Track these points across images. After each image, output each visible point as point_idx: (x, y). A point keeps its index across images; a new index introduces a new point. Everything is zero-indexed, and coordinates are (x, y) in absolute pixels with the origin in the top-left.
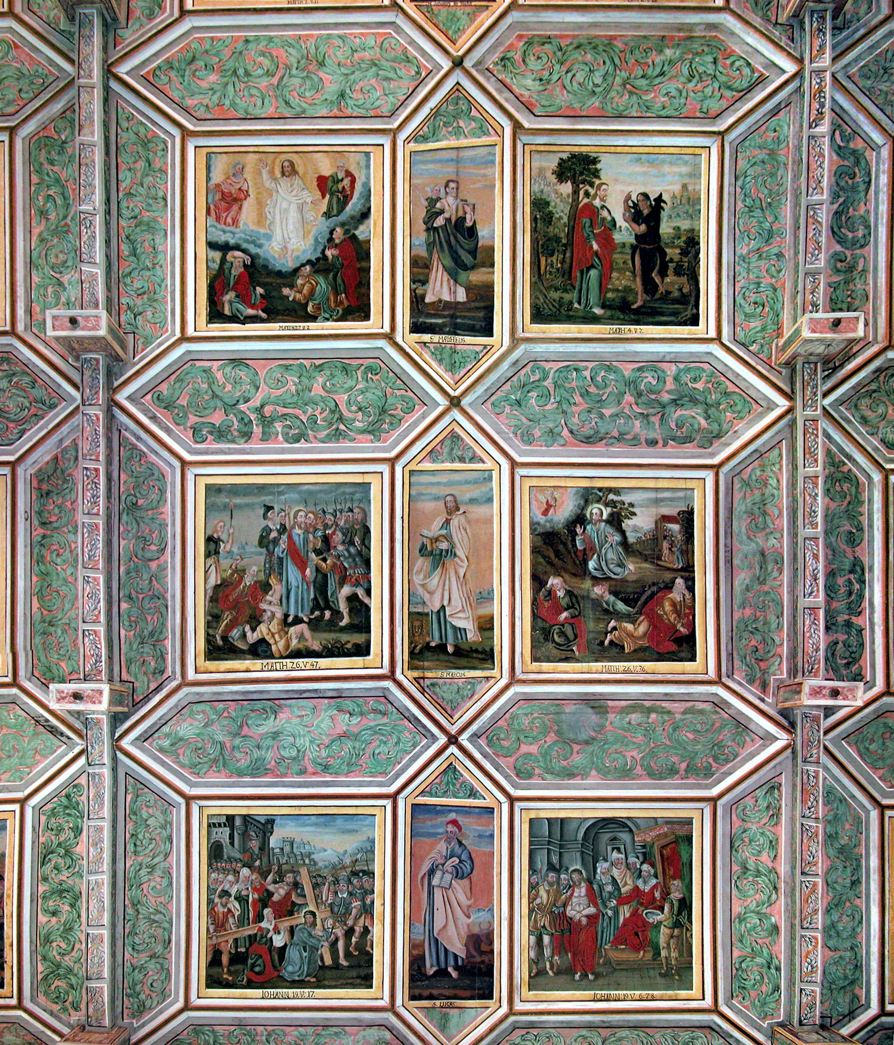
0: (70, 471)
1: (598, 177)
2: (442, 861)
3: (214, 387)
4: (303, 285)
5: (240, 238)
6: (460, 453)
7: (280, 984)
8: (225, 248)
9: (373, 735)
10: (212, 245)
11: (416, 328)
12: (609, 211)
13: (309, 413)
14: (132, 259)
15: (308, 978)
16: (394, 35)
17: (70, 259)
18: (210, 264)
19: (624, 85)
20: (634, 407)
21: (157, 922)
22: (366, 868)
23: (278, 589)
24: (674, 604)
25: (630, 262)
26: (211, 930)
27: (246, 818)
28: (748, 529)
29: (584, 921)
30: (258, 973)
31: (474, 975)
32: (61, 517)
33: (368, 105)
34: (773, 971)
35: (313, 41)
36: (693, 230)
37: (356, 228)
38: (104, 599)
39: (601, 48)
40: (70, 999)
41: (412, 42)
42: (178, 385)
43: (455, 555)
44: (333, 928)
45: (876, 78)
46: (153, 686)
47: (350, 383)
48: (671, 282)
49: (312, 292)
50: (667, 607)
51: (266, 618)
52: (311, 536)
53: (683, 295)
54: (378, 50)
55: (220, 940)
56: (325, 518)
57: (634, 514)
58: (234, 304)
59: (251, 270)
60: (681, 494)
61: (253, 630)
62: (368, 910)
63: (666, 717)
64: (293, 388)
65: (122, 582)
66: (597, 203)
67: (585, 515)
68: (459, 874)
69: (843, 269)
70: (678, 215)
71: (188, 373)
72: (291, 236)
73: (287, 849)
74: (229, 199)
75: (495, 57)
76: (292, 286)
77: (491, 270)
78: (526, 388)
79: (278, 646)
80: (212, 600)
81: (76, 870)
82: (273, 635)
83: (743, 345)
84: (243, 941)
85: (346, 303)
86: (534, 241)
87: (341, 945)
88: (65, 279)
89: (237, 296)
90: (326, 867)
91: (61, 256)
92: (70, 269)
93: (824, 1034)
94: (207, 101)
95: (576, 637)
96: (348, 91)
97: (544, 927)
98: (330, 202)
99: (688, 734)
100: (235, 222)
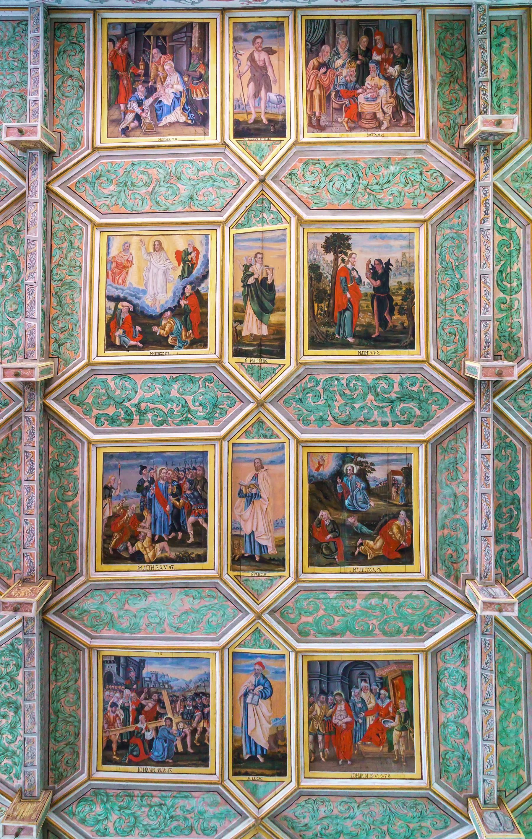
1: (350, 249)
2: (253, 688)
3: (108, 392)
4: (166, 325)
5: (127, 293)
6: (263, 432)
7: (149, 763)
8: (116, 300)
9: (207, 610)
10: (109, 298)
11: (237, 353)
12: (357, 272)
16: (224, 160)
17: (20, 308)
18: (107, 311)
19: (365, 188)
20: (374, 402)
21: (69, 722)
22: (204, 691)
24: (399, 528)
25: (370, 306)
26: (106, 727)
27: (127, 658)
28: (446, 479)
29: (344, 726)
30: (136, 756)
32: (10, 475)
33: (207, 204)
34: (466, 761)
35: (174, 164)
36: (409, 283)
37: (199, 286)
39: (350, 166)
40: (14, 772)
41: (234, 164)
42: (86, 390)
43: (261, 497)
45: (522, 180)
47: (195, 388)
49: (171, 329)
50: (395, 530)
52: (170, 485)
53: (405, 328)
54: (213, 169)
55: (111, 734)
57: (374, 470)
58: (122, 338)
61: (133, 545)
62: (206, 717)
63: (394, 601)
64: (159, 393)
65: (50, 515)
66: (349, 266)
67: (343, 471)
68: (264, 696)
69: (505, 309)
70: (400, 274)
71: (92, 383)
73: (154, 678)
75: (287, 172)
76: (159, 325)
77: (283, 313)
78: (306, 391)
79: (149, 555)
81: (18, 690)
86: (310, 293)
87: (188, 739)
88: (16, 322)
89: (124, 332)
90: (179, 690)
91: (14, 306)
95: (337, 549)
96: (195, 195)
97: (318, 729)
100: (124, 282)
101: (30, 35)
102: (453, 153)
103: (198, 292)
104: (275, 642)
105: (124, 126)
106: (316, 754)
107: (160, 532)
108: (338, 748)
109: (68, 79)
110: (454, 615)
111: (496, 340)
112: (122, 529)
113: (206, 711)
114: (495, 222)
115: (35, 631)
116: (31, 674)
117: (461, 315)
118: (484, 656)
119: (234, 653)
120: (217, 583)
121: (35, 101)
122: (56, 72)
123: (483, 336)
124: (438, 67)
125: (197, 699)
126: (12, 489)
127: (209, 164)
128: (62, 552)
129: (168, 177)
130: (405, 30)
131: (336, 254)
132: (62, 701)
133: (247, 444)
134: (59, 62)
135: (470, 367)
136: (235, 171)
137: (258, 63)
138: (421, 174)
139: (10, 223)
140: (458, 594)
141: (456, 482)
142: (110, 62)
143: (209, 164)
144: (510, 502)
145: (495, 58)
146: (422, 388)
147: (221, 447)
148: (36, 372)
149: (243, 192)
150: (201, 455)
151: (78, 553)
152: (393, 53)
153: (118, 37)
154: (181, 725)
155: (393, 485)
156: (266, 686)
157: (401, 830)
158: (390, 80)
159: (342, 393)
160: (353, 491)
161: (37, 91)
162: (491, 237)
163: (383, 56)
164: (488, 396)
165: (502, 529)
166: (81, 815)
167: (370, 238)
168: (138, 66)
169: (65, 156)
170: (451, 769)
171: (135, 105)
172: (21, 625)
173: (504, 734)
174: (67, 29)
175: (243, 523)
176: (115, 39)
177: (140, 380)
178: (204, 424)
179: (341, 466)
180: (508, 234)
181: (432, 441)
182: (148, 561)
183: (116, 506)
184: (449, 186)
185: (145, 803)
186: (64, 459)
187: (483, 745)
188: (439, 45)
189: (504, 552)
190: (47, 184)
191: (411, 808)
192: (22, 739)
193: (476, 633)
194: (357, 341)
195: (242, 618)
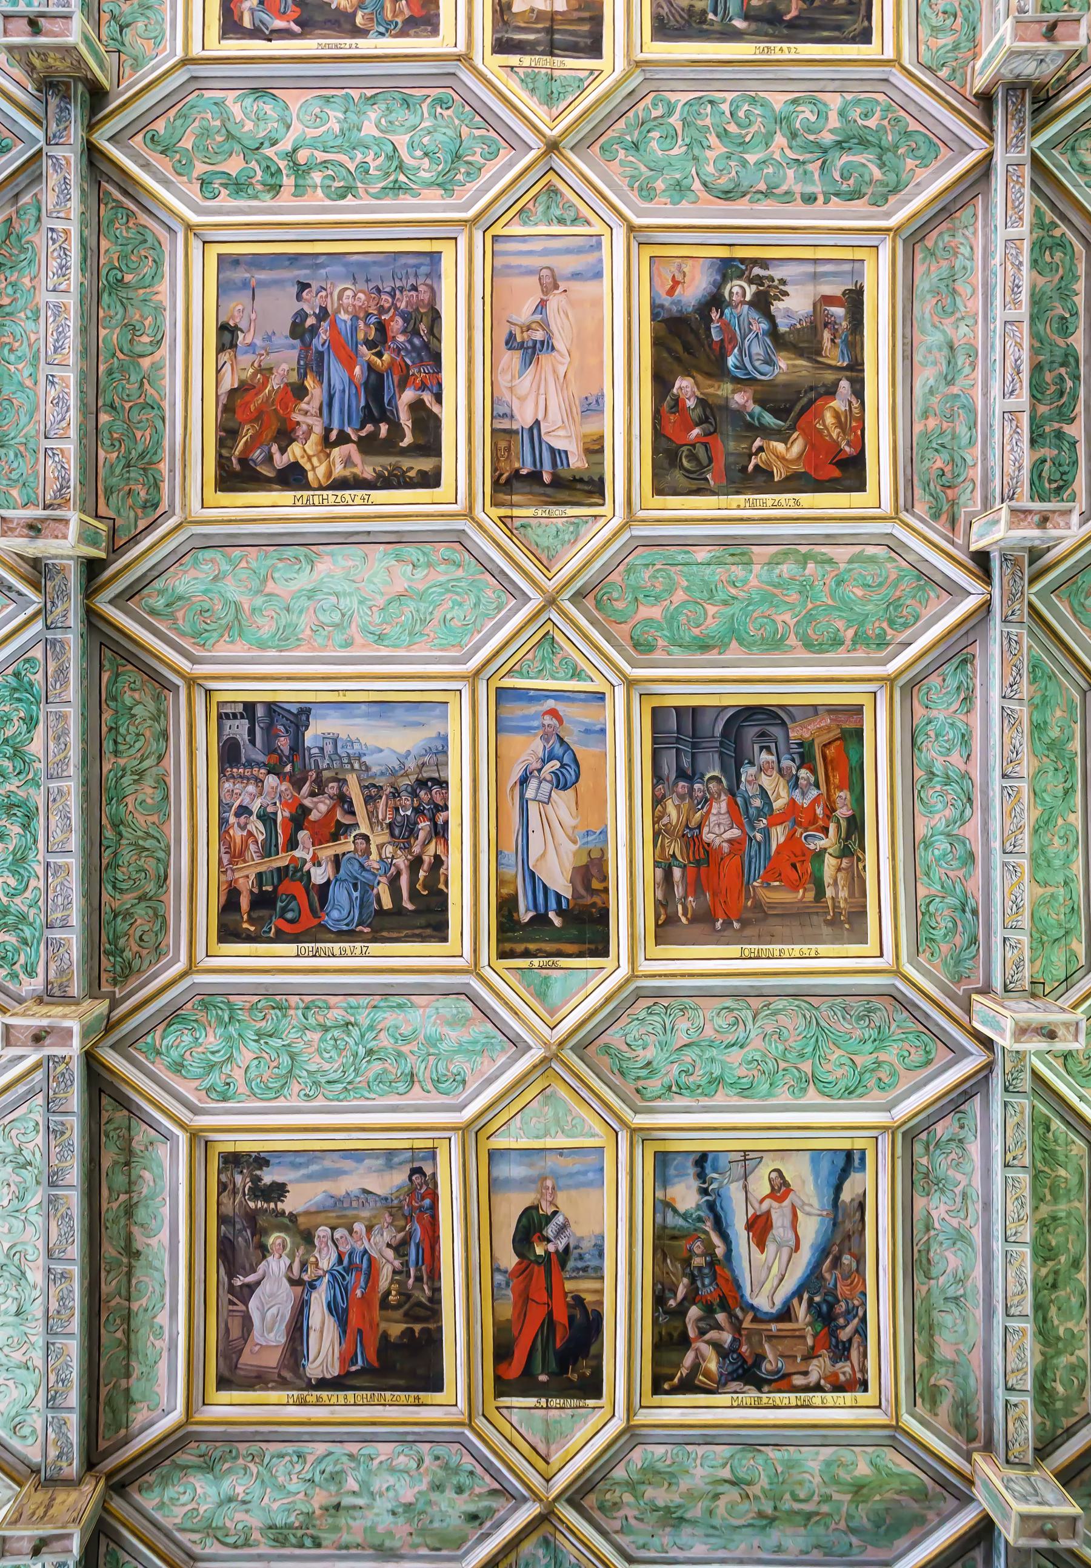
2: (539, 766)
6: (558, 213)
9: (443, 594)
11: (502, 46)
15: (360, 928)
20: (787, 151)
21: (147, 850)
22: (436, 775)
23: (316, 392)
24: (837, 415)
26: (225, 862)
30: (291, 921)
31: (583, 922)
34: (969, 915)
38: (75, 406)
40: (22, 961)
42: (179, 122)
43: (553, 348)
44: (393, 858)
46: (142, 524)
47: (413, 120)
50: (829, 419)
51: (299, 433)
52: (361, 324)
55: (237, 875)
56: (380, 298)
57: (786, 294)
60: (847, 267)
61: (283, 450)
62: (440, 832)
63: (828, 568)
64: (337, 128)
65: (101, 386)
68: (561, 783)
71: (192, 107)
73: (329, 749)
78: (646, 127)
79: (317, 472)
81: (31, 776)
82: (309, 458)
83: (929, 68)
84: (269, 875)
85: (407, 13)
90: (382, 774)
93: (1037, 1003)
95: (711, 460)
97: (674, 856)
99: (856, 590)
104: (582, 664)
106: (670, 910)
108: (714, 895)
110: (946, 598)
112: (259, 417)
113: (440, 820)
115: (71, 621)
116: (61, 717)
125: (422, 794)
126: (18, 330)
128: (128, 465)
132: (130, 800)
141: (953, 319)
146: (885, 123)
150: (427, 260)
151: (164, 467)
154: (389, 850)
155: (826, 325)
156: (566, 760)
157: (840, 1072)
160: (743, 338)
166: (174, 1054)
170: (938, 934)
177: (295, 100)
179: (719, 286)
183: (245, 366)
185: (312, 1021)
187: (1005, 864)
191: (860, 1018)
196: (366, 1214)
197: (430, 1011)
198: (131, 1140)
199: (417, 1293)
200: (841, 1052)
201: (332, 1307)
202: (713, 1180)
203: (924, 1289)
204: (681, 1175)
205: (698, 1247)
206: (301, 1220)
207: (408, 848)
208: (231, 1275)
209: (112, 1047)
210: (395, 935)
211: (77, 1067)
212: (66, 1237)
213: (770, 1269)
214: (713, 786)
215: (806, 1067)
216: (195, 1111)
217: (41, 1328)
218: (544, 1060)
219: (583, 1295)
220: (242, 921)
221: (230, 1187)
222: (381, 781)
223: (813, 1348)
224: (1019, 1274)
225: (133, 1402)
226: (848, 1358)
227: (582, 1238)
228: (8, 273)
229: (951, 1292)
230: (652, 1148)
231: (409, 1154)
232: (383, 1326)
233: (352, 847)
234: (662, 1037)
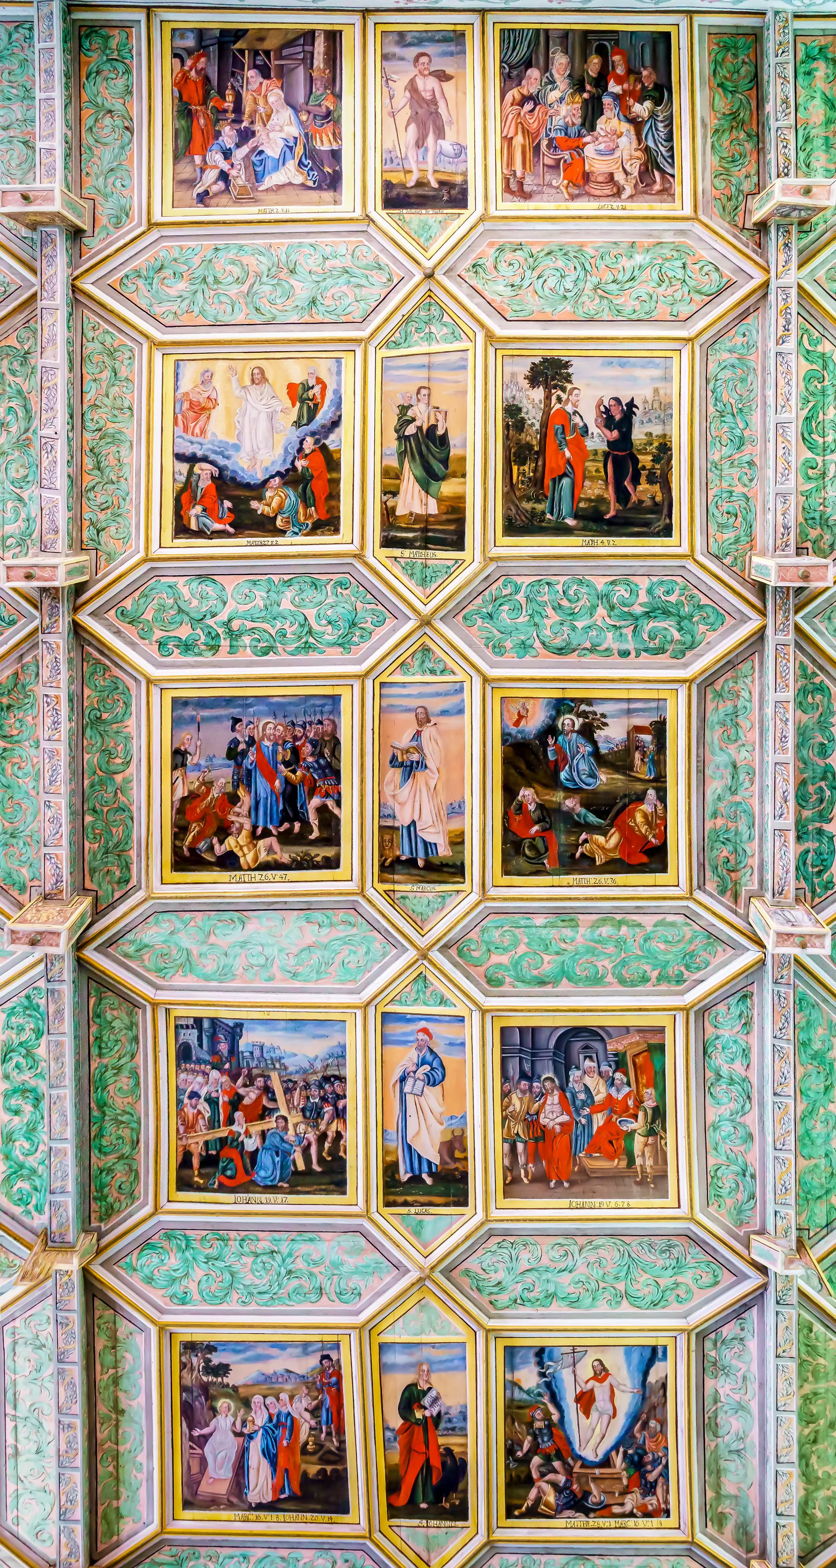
0: (31, 687)
1: (570, 382)
2: (414, 1069)
3: (179, 602)
4: (272, 498)
5: (209, 449)
6: (430, 665)
7: (252, 1188)
8: (192, 459)
11: (387, 543)
13: (278, 627)
14: (96, 472)
15: (280, 1184)
16: (366, 243)
17: (31, 474)
18: (177, 476)
19: (596, 288)
20: (607, 619)
21: (123, 1122)
22: (337, 1073)
23: (246, 799)
24: (645, 816)
25: (602, 470)
27: (214, 1021)
28: (721, 740)
29: (558, 1128)
30: (230, 1177)
31: (448, 1181)
34: (748, 1178)
35: (284, 249)
36: (665, 436)
37: (326, 437)
39: (572, 254)
40: (34, 1202)
41: (384, 249)
42: (142, 600)
43: (426, 767)
46: (117, 895)
47: (320, 597)
48: (645, 492)
49: (281, 506)
50: (639, 818)
51: (234, 829)
52: (280, 749)
53: (656, 504)
54: (349, 257)
55: (190, 1141)
57: (606, 724)
58: (201, 519)
59: (219, 482)
60: (653, 705)
61: (221, 842)
62: (340, 1114)
63: (637, 930)
64: (261, 604)
65: (86, 794)
66: (569, 408)
67: (556, 726)
68: (431, 1081)
69: (814, 476)
70: (650, 421)
71: (152, 589)
72: (261, 446)
73: (257, 1053)
74: (196, 409)
75: (469, 262)
76: (260, 499)
77: (462, 480)
78: (498, 602)
79: (247, 858)
80: (179, 811)
81: (39, 1071)
82: (241, 848)
86: (507, 449)
87: (313, 1150)
88: (25, 496)
89: (204, 510)
90: (297, 1072)
92: (30, 485)
94: (176, 307)
96: (319, 297)
97: (517, 1134)
98: (301, 408)
100: (203, 432)
101: (38, 46)
102: (735, 236)
103: (324, 448)
104: (448, 995)
105: (201, 190)
106: (515, 1173)
107: (266, 822)
108: (549, 1163)
109: (104, 115)
111: (801, 524)
112: (203, 818)
113: (341, 1105)
114: (800, 343)
117: (745, 485)
118: (777, 1017)
119: (384, 1015)
120: (357, 901)
121: (50, 151)
122: (84, 105)
123: (780, 518)
124: (712, 105)
125: (327, 1087)
126: (24, 754)
127: (342, 250)
128: (106, 852)
129: (274, 269)
130: (661, 48)
131: (548, 388)
132: (111, 1088)
133: (404, 684)
134: (90, 89)
135: (758, 566)
136: (384, 259)
137: (423, 94)
138: (684, 267)
139: (12, 341)
140: (738, 919)
142: (176, 89)
143: (342, 250)
144: (820, 776)
145: (801, 92)
146: (683, 598)
147: (363, 689)
148: (61, 572)
149: (398, 292)
150: (330, 702)
151: (133, 854)
152: (641, 81)
153: (189, 52)
154: (302, 1128)
155: (637, 748)
157: (646, 1290)
158: (637, 124)
159: (556, 604)
160: (572, 759)
161: (52, 135)
162: (793, 365)
163: (626, 86)
164: (787, 611)
165: (807, 819)
166: (147, 1271)
167: (603, 365)
168: (223, 97)
169: (102, 236)
170: (724, 1192)
171: (219, 157)
172: (42, 967)
173: (807, 1141)
174: (102, 36)
175: (397, 808)
176: (184, 55)
177: (230, 584)
178: (335, 653)
179: (554, 719)
180: (820, 361)
181: (698, 681)
182: (246, 867)
183: (194, 779)
184: (728, 286)
185: (246, 1249)
186: (108, 707)
187: (776, 1158)
188: (714, 71)
189: (810, 855)
190: (74, 280)
191: (663, 1252)
192: (46, 1149)
193: (765, 981)
194: (581, 524)
195: (397, 958)
196: (288, 1387)
197: (334, 1244)
198: (116, 1331)
199: (328, 1444)
200: (648, 1276)
201: (266, 1453)
202: (549, 1367)
203: (713, 1445)
204: (525, 1362)
205: (538, 1414)
206: (241, 1390)
207: (316, 1126)
208: (191, 1428)
209: (101, 1265)
210: (307, 1189)
211: (76, 1279)
212: (72, 1399)
213: (593, 1430)
214: (548, 1084)
215: (621, 1286)
216: (162, 1311)
217: (54, 1463)
218: (420, 1280)
219: (452, 1448)
220: (193, 1176)
221: (189, 1366)
222: (295, 1078)
223: (628, 1486)
224: (787, 1434)
225: (122, 1517)
226: (654, 1494)
227: (450, 1407)
228: (16, 712)
229: (734, 1447)
230: (502, 1343)
231: (320, 1345)
232: (304, 1466)
233: (274, 1125)
234: (509, 1265)
